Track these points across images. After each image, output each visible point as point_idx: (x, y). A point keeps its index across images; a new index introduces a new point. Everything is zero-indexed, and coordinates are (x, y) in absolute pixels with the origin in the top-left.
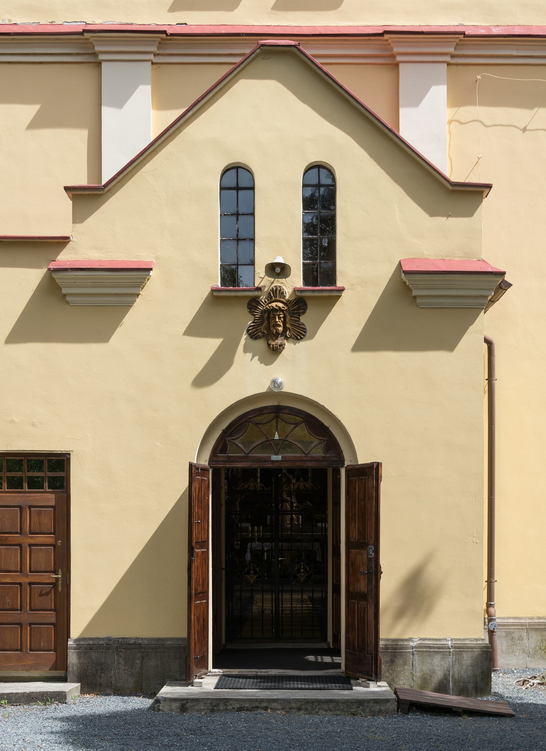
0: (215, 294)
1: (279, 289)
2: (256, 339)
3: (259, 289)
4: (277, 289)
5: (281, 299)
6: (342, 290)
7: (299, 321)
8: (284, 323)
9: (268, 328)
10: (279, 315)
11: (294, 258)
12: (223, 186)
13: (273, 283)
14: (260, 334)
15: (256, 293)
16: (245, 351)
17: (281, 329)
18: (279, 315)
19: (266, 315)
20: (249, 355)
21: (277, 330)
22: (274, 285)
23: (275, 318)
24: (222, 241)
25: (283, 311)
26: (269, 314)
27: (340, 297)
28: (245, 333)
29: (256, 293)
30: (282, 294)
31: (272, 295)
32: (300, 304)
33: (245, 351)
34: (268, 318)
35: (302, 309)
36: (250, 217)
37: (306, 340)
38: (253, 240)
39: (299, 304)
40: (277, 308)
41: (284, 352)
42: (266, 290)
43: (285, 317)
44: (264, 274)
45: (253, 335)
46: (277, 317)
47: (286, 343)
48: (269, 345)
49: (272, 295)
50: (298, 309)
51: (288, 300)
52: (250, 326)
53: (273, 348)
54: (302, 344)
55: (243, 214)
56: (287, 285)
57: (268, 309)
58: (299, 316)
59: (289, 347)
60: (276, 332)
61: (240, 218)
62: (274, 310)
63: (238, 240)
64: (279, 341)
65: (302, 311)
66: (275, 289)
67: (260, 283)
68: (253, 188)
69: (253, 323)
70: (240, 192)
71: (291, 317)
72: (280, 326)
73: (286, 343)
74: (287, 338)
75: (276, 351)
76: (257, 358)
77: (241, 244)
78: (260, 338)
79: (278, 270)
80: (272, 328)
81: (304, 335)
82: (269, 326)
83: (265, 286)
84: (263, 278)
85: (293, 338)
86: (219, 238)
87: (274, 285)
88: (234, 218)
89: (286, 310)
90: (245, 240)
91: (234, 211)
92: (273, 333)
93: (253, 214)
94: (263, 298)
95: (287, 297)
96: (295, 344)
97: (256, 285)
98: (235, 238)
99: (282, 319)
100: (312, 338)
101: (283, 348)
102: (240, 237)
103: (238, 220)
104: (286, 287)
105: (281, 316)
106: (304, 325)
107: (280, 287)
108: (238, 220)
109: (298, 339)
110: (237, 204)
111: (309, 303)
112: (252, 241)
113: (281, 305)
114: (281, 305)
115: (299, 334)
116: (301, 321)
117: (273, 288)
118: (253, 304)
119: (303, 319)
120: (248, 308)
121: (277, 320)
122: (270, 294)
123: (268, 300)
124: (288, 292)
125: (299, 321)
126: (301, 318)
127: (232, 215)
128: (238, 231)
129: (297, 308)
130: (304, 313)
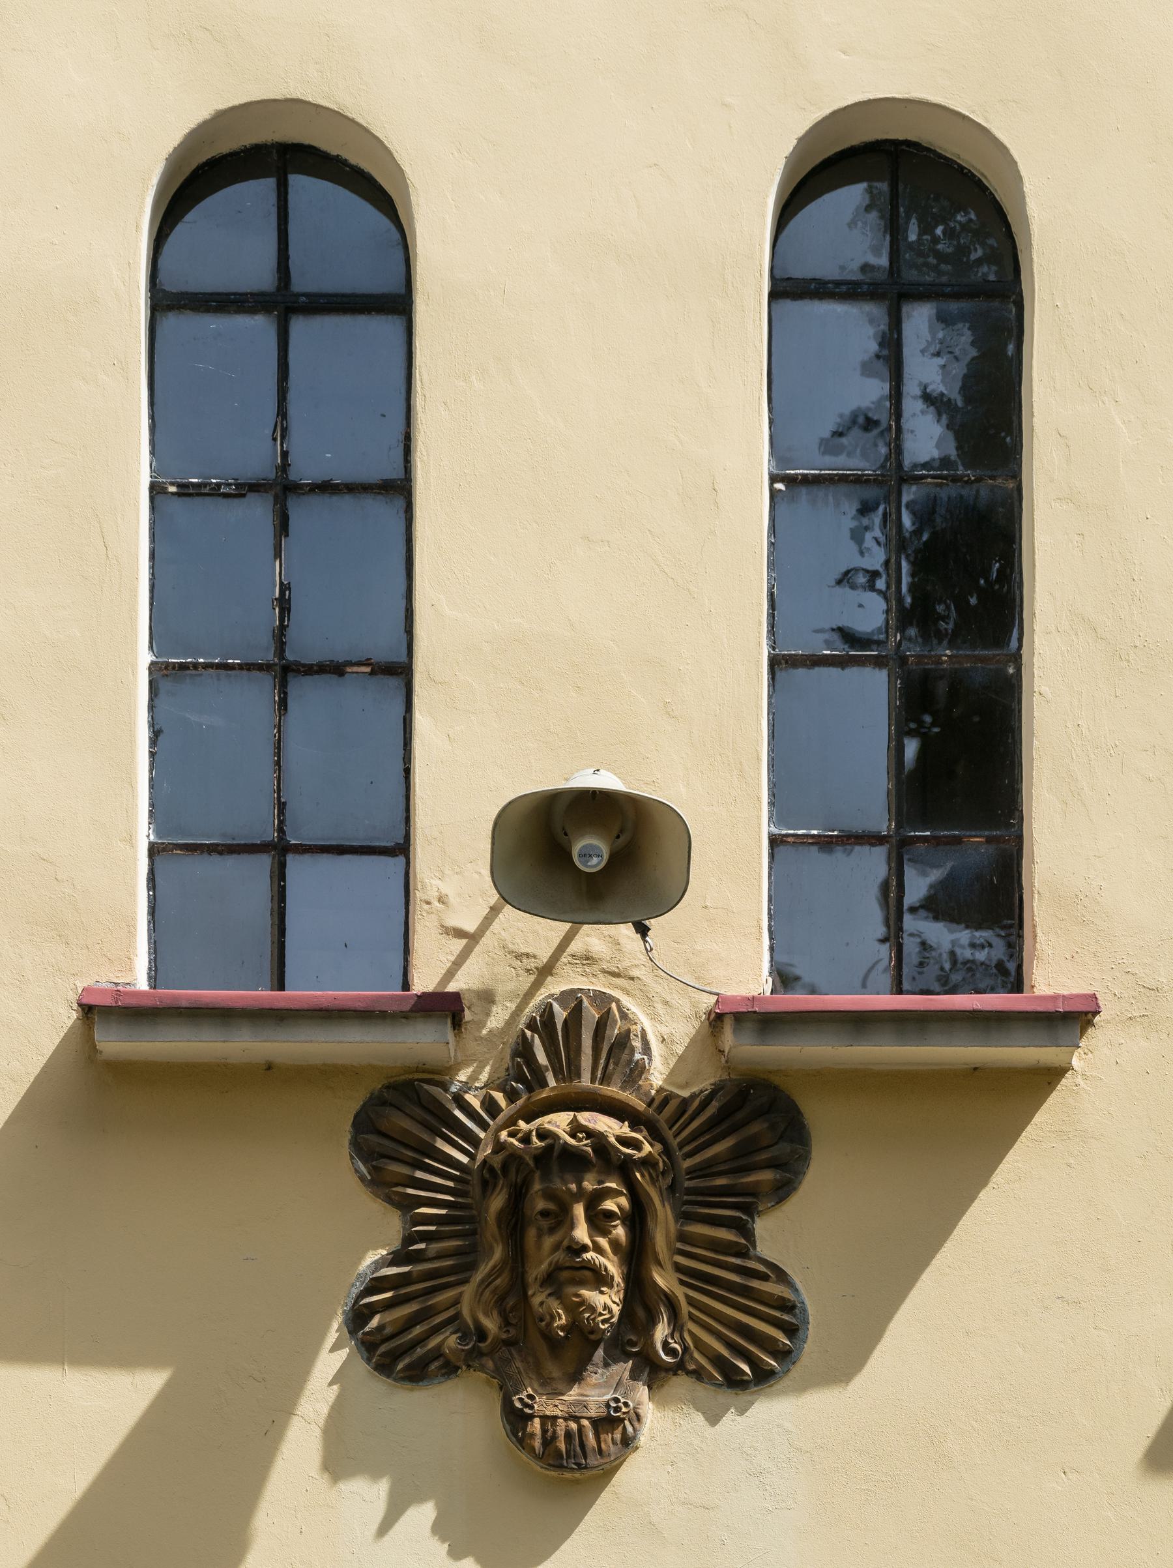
0: (115, 1043)
1: (591, 1014)
2: (417, 1375)
3: (446, 1008)
4: (576, 1013)
5: (613, 1090)
6: (1072, 1019)
7: (743, 1253)
8: (636, 1256)
9: (512, 1298)
10: (593, 1201)
11: (706, 746)
12: (171, 284)
13: (546, 971)
14: (450, 1341)
15: (422, 1042)
16: (340, 1460)
17: (606, 1301)
18: (593, 1201)
19: (497, 1202)
20: (368, 1495)
21: (577, 1308)
22: (555, 987)
23: (561, 1218)
24: (162, 675)
25: (624, 1169)
26: (518, 1196)
27: (1052, 1076)
28: (332, 1336)
29: (422, 1042)
30: (620, 1051)
31: (542, 1058)
32: (756, 1128)
33: (340, 1460)
34: (515, 1222)
35: (773, 1164)
36: (383, 510)
37: (802, 1388)
38: (399, 672)
39: (745, 1128)
40: (584, 1145)
41: (633, 1475)
42: (497, 1018)
43: (637, 1218)
44: (494, 897)
45: (398, 1343)
46: (579, 1210)
47: (649, 1410)
48: (516, 1419)
49: (542, 1058)
50: (741, 1160)
51: (665, 1099)
52: (376, 1285)
53: (549, 1441)
54: (773, 1418)
55: (326, 488)
56: (659, 987)
57: (512, 1159)
58: (750, 1210)
59: (670, 1432)
60: (574, 1327)
61: (301, 512)
62: (558, 1158)
63: (285, 672)
64: (595, 1392)
65: (766, 1176)
66: (560, 1014)
67: (450, 974)
68: (397, 304)
69: (396, 1259)
70: (300, 327)
71: (685, 1217)
72: (600, 1279)
73: (649, 1410)
74: (652, 1371)
75: (575, 1463)
76: (423, 1514)
77: (308, 696)
78: (450, 1369)
79: (588, 851)
80: (538, 1297)
81: (784, 1355)
82: (519, 1284)
83: (487, 998)
84: (473, 939)
85: (698, 1374)
86: (145, 658)
87: (555, 987)
88: (257, 513)
89: (647, 1163)
90: (336, 669)
91: (255, 458)
92: (548, 1337)
93: (399, 489)
94: (474, 1078)
95: (657, 1076)
96: (714, 1419)
97: (424, 981)
98: (268, 655)
99: (620, 1232)
100: (844, 1367)
101: (628, 1442)
102: (307, 644)
103: (283, 526)
104: (648, 1001)
105: (610, 1205)
106: (782, 1276)
107: (601, 999)
108: (283, 526)
109: (734, 1382)
110: (282, 411)
111: (820, 1115)
112: (394, 682)
113: (609, 1126)
114: (609, 1126)
115: (751, 1343)
116: (765, 1249)
117: (547, 1013)
118: (397, 1123)
119: (775, 1235)
120: (360, 1149)
121: (582, 1233)
122: (523, 1050)
123: (512, 1096)
124: (665, 1041)
125: (742, 1253)
126: (762, 1226)
127: (246, 489)
128: (284, 604)
129: (738, 1152)
130: (783, 1190)
